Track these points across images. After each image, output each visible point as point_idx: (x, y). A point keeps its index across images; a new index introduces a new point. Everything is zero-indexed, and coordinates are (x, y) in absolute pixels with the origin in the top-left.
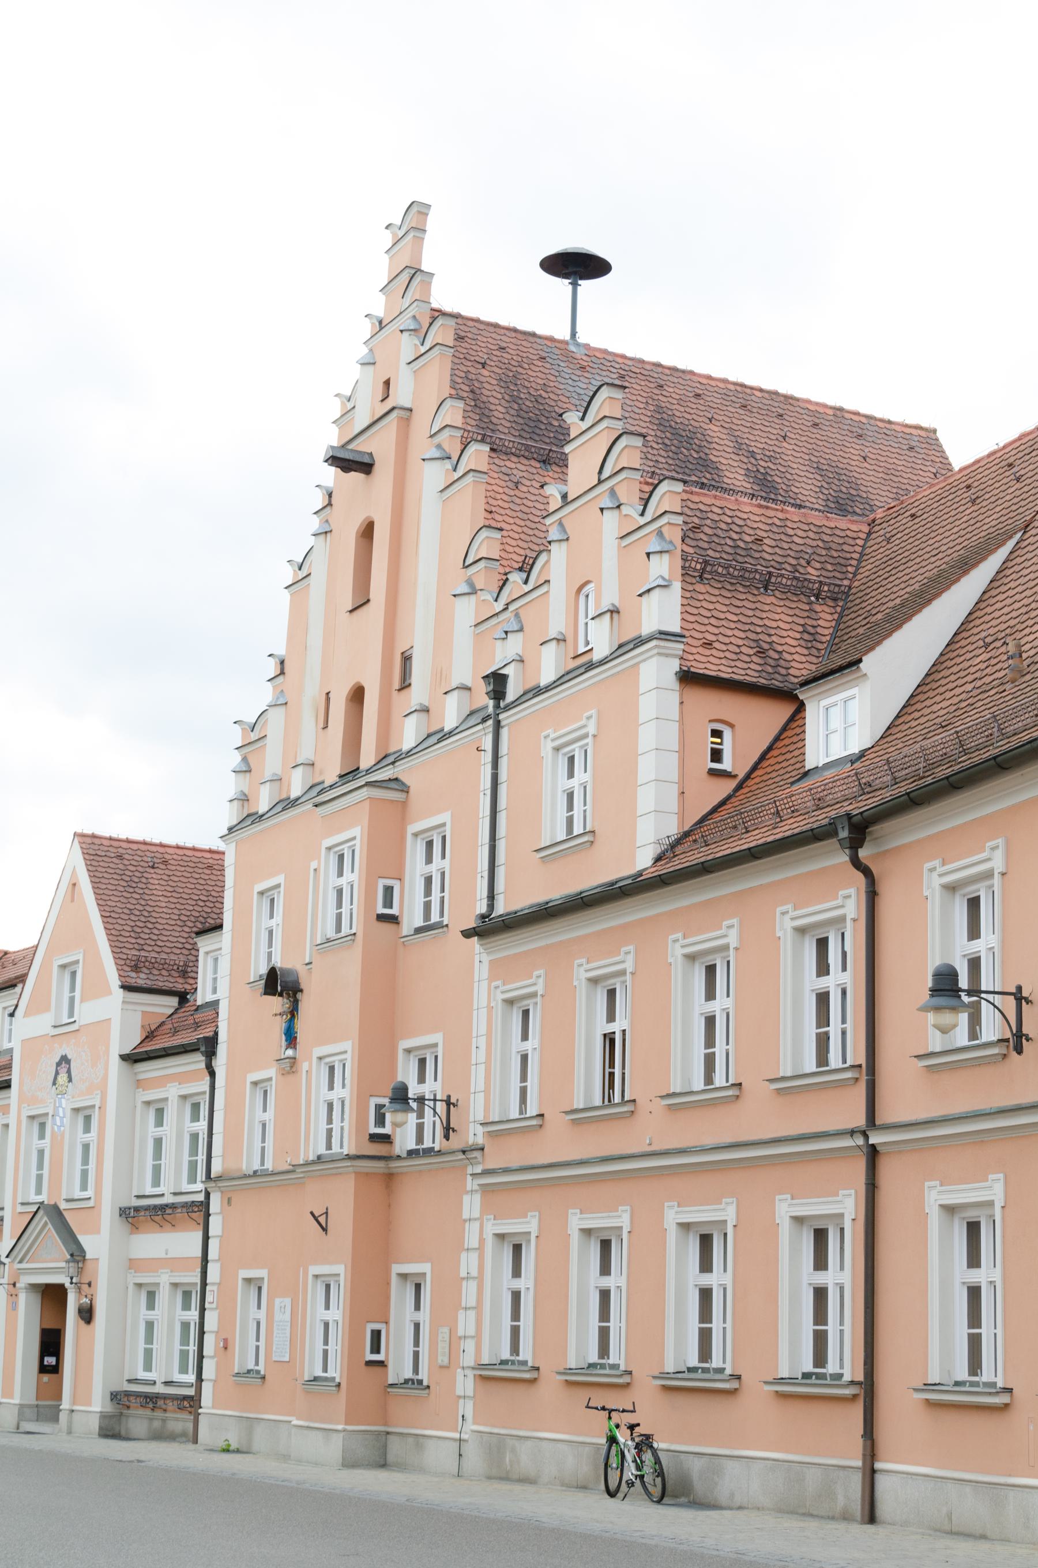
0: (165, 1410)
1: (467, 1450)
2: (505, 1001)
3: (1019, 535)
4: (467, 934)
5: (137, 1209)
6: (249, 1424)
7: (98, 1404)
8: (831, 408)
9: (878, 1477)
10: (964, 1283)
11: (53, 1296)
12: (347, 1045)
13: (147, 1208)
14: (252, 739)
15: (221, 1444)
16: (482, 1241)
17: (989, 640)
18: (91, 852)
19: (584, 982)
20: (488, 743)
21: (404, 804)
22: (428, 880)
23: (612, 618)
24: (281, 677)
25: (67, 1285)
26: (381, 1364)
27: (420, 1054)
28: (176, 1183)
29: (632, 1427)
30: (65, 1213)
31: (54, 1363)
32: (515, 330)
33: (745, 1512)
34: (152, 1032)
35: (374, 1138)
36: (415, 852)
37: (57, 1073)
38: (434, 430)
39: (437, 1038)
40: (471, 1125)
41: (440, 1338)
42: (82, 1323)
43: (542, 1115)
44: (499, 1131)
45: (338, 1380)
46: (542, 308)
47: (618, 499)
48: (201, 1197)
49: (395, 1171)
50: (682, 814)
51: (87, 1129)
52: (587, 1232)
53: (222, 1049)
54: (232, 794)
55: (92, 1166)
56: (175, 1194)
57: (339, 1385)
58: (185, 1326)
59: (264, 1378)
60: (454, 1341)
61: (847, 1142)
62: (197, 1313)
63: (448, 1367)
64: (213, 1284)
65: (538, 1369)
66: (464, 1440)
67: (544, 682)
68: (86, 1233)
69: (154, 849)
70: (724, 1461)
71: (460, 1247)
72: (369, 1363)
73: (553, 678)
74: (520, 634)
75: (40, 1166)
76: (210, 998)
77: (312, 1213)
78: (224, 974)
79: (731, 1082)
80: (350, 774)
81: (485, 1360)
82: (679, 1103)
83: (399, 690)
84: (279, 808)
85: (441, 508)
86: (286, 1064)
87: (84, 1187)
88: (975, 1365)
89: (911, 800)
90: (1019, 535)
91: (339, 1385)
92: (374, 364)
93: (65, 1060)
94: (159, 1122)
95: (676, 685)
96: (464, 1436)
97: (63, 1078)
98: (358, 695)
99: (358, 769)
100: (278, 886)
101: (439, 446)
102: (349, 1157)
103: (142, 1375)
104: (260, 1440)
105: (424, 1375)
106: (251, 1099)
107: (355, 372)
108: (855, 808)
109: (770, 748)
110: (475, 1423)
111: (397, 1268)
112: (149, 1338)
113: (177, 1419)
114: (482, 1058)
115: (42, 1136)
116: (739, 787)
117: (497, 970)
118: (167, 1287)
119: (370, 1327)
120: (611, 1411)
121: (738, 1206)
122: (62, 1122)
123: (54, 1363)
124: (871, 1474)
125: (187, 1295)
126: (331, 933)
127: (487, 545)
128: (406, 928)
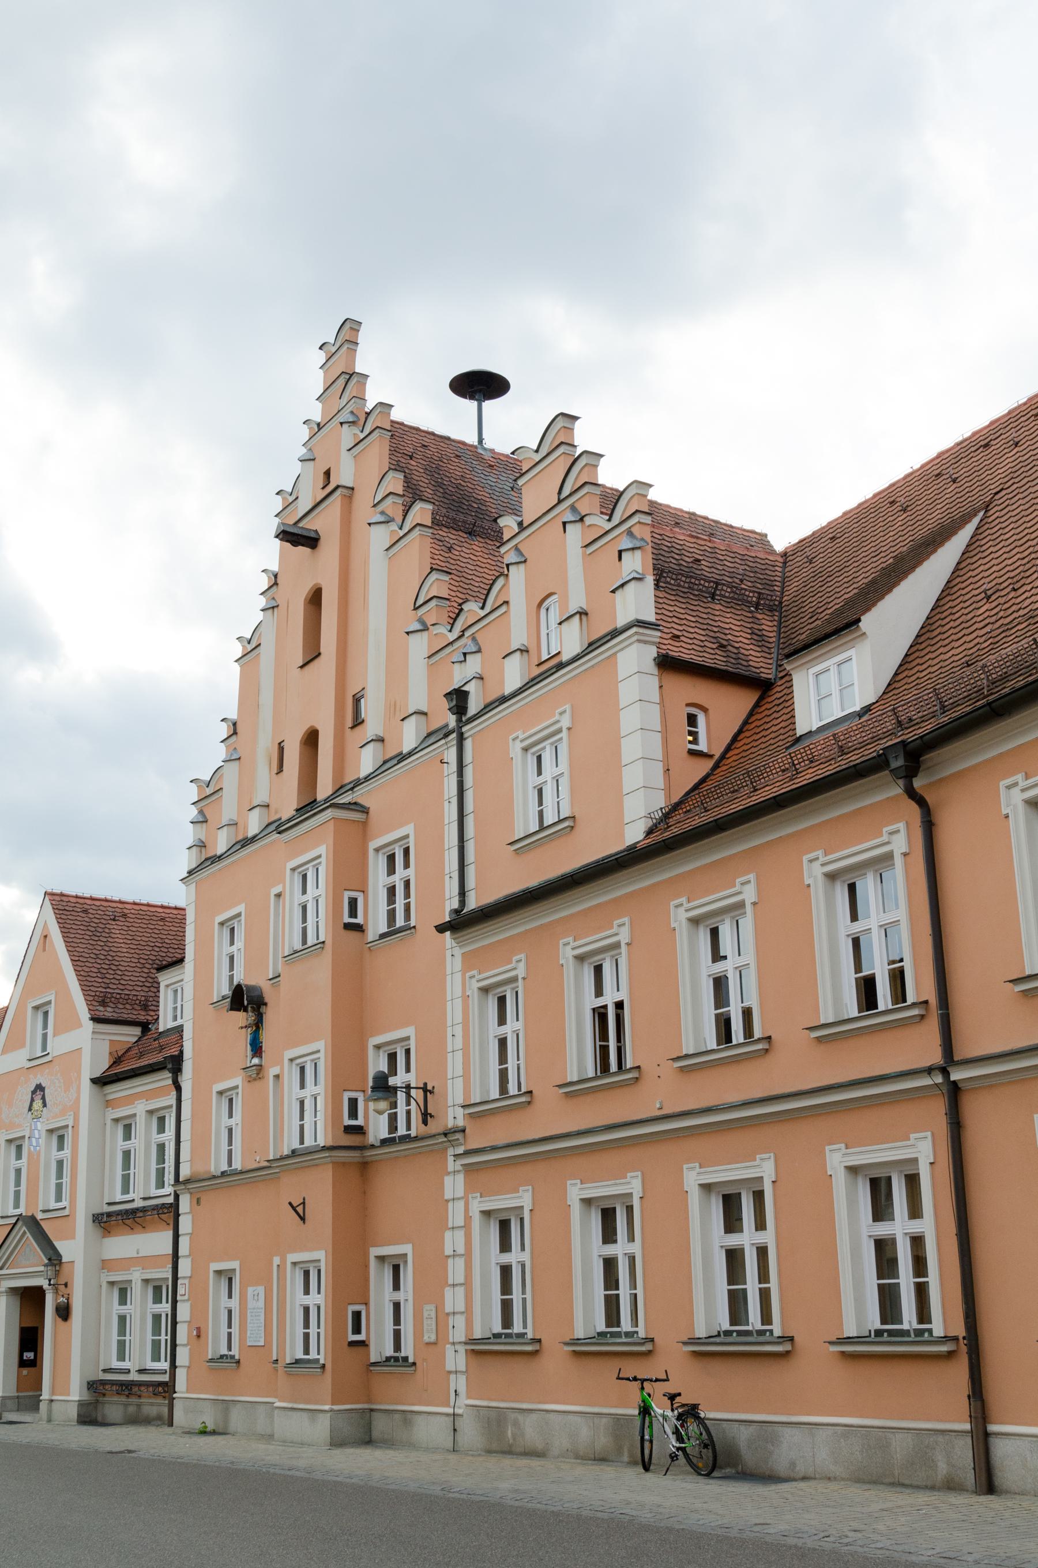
0: (140, 1396)
1: (462, 1424)
2: (481, 989)
3: (982, 513)
4: (441, 929)
5: (109, 1215)
6: (226, 1406)
7: (76, 1393)
8: (686, 512)
9: (994, 1442)
10: (870, 1236)
11: (31, 1299)
12: (320, 1045)
13: (119, 1213)
14: (209, 794)
15: (198, 1426)
16: (468, 1218)
17: (989, 593)
18: (60, 907)
19: (571, 960)
20: (451, 755)
21: (365, 824)
22: (392, 891)
23: (581, 619)
24: (234, 737)
25: (46, 1286)
26: (363, 1344)
27: (390, 1049)
28: (145, 1189)
29: (672, 1397)
30: (42, 1223)
31: (25, 1354)
32: (433, 434)
33: (812, 1483)
34: (120, 1058)
35: (349, 1130)
36: (377, 866)
37: (32, 1100)
38: (378, 499)
39: (409, 1031)
40: (450, 1110)
41: (426, 1314)
42: (59, 1320)
43: (639, 1067)
44: (479, 1112)
45: (322, 1362)
46: (454, 419)
47: (579, 513)
48: (171, 1200)
49: (369, 1159)
50: (668, 789)
51: (61, 1148)
52: (587, 1202)
53: (187, 1066)
54: (190, 843)
55: (66, 1180)
56: (145, 1199)
57: (323, 1366)
58: (157, 1318)
59: (238, 1362)
60: (442, 1318)
61: (927, 1081)
62: (169, 1305)
63: (435, 1344)
64: (184, 1278)
65: (539, 1341)
66: (458, 1415)
67: (508, 691)
68: (61, 1239)
69: (114, 905)
70: (779, 1429)
71: (443, 1225)
72: (352, 1344)
73: (518, 685)
74: (479, 655)
75: (18, 1183)
76: (171, 1024)
77: (290, 1204)
78: (186, 1001)
79: (523, 1090)
80: (308, 807)
81: (477, 1335)
82: (690, 1065)
83: (352, 728)
84: (238, 846)
85: (388, 564)
86: (253, 1072)
87: (59, 1199)
88: (507, 1320)
89: (992, 710)
90: (982, 513)
91: (323, 1366)
92: (314, 460)
93: (40, 1088)
94: (127, 1136)
95: (655, 671)
96: (458, 1411)
97: (38, 1104)
98: (311, 739)
99: (315, 800)
100: (239, 915)
101: (382, 513)
102: (325, 1148)
103: (116, 1364)
104: (237, 1419)
105: (408, 1350)
106: (218, 1108)
107: (297, 468)
108: (910, 735)
109: (740, 731)
110: (469, 1397)
111: (375, 1252)
112: (122, 1331)
113: (152, 1404)
114: (459, 1043)
115: (19, 1156)
116: (716, 766)
117: (469, 961)
118: (139, 1282)
119: (351, 1308)
120: (643, 1381)
121: (776, 1161)
122: (39, 1143)
123: (25, 1354)
124: (982, 1440)
125: (157, 1290)
126: (298, 946)
127: (438, 585)
128: (371, 935)
